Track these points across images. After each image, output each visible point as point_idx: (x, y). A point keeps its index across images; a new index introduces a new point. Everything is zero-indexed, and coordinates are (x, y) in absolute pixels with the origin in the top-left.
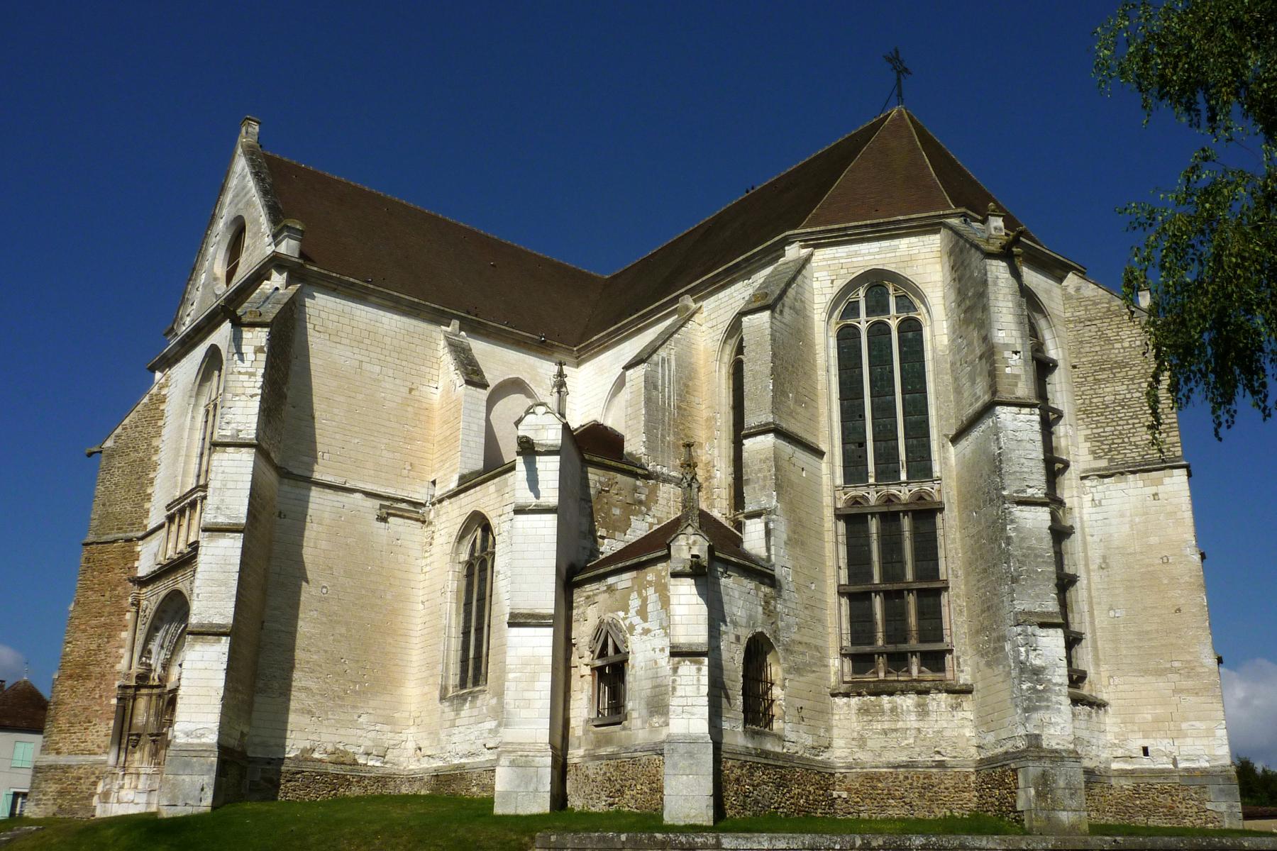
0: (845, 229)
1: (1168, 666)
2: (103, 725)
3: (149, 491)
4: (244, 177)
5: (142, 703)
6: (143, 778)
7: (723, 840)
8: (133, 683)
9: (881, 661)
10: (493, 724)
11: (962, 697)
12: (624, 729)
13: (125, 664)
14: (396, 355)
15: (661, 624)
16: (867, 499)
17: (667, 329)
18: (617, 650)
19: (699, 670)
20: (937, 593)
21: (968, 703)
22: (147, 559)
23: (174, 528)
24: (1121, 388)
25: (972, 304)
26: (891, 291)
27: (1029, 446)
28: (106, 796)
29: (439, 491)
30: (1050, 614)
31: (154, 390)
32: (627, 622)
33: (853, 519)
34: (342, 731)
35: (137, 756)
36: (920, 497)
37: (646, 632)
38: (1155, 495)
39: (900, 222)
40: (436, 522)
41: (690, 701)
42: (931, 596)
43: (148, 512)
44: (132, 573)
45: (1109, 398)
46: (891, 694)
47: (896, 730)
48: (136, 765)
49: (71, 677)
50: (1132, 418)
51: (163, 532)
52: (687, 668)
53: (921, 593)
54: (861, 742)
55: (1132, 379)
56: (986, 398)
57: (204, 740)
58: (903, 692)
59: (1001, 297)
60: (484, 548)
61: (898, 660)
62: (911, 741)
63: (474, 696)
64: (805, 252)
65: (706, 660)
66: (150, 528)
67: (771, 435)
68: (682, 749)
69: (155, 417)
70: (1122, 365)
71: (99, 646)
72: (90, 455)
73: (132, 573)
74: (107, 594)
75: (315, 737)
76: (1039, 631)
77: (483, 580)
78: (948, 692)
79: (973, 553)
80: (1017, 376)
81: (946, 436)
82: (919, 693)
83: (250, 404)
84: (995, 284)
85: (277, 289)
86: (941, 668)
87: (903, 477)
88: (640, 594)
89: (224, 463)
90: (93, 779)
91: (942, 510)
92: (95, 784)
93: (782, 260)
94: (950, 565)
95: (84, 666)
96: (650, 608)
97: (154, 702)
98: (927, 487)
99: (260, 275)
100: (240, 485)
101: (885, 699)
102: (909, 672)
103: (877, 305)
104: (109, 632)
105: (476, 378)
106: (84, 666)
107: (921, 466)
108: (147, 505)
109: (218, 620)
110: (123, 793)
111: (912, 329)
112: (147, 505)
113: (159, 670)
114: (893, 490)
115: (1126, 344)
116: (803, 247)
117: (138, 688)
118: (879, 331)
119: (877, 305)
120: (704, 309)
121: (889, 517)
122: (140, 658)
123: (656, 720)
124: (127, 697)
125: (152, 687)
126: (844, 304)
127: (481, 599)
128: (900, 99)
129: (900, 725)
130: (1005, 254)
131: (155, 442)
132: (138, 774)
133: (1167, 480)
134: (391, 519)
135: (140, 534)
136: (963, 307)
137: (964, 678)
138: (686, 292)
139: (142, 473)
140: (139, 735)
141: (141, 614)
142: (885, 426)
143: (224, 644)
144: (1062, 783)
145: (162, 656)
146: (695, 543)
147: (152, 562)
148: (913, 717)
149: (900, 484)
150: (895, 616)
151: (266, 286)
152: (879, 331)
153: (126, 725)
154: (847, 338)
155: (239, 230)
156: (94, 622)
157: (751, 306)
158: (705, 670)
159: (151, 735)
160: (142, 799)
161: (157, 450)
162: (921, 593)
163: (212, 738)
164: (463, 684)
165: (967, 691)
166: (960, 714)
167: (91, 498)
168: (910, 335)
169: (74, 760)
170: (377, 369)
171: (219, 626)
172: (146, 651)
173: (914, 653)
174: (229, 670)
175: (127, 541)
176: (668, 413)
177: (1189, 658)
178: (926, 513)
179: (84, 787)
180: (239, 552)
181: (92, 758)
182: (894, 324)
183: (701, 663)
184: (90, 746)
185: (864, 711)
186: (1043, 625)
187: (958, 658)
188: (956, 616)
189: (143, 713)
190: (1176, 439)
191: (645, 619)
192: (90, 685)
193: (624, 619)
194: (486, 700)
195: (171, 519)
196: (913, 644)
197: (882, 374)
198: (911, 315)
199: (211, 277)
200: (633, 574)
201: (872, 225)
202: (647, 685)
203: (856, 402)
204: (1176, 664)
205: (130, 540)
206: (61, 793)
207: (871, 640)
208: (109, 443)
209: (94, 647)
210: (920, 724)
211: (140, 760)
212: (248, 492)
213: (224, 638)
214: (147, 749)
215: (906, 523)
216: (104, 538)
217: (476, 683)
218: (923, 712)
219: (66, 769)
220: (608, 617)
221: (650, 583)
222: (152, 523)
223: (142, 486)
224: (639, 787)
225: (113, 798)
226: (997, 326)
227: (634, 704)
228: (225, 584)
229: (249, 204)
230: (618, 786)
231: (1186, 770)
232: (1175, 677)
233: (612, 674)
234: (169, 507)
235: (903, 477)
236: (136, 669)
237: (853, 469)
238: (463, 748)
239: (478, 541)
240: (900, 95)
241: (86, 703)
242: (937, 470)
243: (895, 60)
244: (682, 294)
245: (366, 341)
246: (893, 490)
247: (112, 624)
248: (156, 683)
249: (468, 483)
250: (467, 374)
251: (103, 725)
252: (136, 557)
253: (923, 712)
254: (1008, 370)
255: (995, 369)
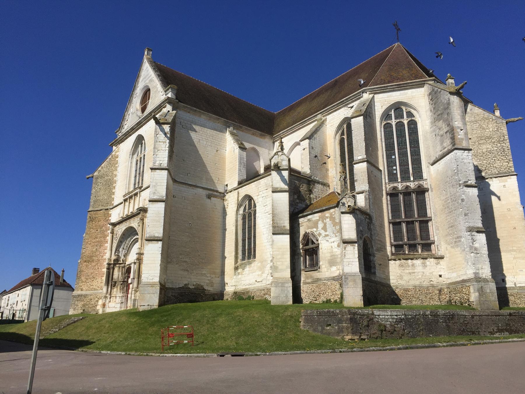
0: (387, 86)
1: (511, 249)
2: (100, 279)
3: (113, 191)
4: (148, 71)
5: (116, 269)
6: (118, 298)
7: (375, 312)
8: (112, 262)
9: (406, 248)
10: (260, 273)
11: (440, 260)
12: (319, 272)
13: (107, 254)
14: (211, 137)
15: (333, 233)
16: (398, 188)
17: (314, 127)
18: (313, 243)
19: (354, 248)
20: (427, 222)
21: (442, 262)
22: (115, 216)
23: (127, 204)
24: (489, 146)
25: (440, 112)
26: (404, 110)
27: (468, 164)
28: (104, 305)
29: (229, 188)
30: (481, 228)
31: (113, 153)
32: (318, 232)
33: (393, 195)
34: (199, 277)
35: (115, 290)
36: (420, 186)
37: (327, 235)
38: (504, 186)
39: (408, 83)
40: (229, 199)
41: (351, 260)
42: (425, 223)
43: (113, 199)
44: (109, 222)
45: (484, 150)
46: (412, 259)
47: (414, 273)
48: (115, 293)
49: (85, 261)
50: (494, 157)
51: (123, 204)
52: (349, 247)
53: (421, 222)
54: (401, 277)
55: (494, 143)
56: (450, 147)
57: (154, 281)
58: (417, 259)
59: (455, 109)
60: (250, 208)
61: (413, 247)
62: (420, 276)
63: (250, 263)
64: (371, 96)
65: (356, 245)
66: (115, 205)
67: (366, 163)
68: (350, 278)
69: (114, 164)
70: (489, 138)
71: (96, 249)
72: (88, 178)
73: (109, 222)
74: (99, 230)
75: (189, 280)
76: (476, 234)
77: (250, 220)
78: (434, 258)
79: (443, 206)
80: (462, 139)
81: (429, 163)
82: (423, 259)
83: (164, 153)
84: (453, 104)
85: (169, 111)
86: (430, 250)
87: (412, 179)
88: (323, 221)
89: (156, 176)
90: (96, 299)
91: (428, 191)
92: (97, 301)
93: (361, 99)
94: (432, 211)
95: (91, 257)
96: (328, 226)
97: (121, 270)
98: (421, 182)
99: (160, 107)
100: (162, 184)
101: (410, 261)
102: (417, 251)
103: (399, 115)
104: (101, 244)
105: (242, 146)
106: (91, 257)
107: (418, 174)
108: (113, 196)
109: (157, 235)
110: (110, 304)
111: (413, 125)
112: (113, 196)
113: (122, 257)
114: (408, 184)
115: (491, 130)
116: (370, 94)
117: (115, 264)
118: (400, 125)
119: (399, 115)
120: (327, 119)
121: (407, 193)
122: (115, 253)
123: (334, 268)
124: (110, 268)
125: (120, 264)
126: (386, 115)
127: (250, 227)
128: (398, 40)
129: (415, 271)
130: (457, 93)
131: (115, 173)
132: (116, 297)
133: (509, 180)
134: (212, 198)
135: (111, 207)
136: (437, 114)
137: (440, 253)
138: (320, 113)
139: (110, 185)
140: (115, 282)
141: (115, 236)
142: (404, 160)
143: (160, 244)
144: (488, 291)
145: (123, 252)
146: (349, 201)
147: (118, 217)
148: (421, 268)
149: (411, 181)
150: (411, 231)
151: (165, 110)
152: (400, 125)
153: (110, 279)
154: (387, 128)
155: (147, 93)
156: (94, 241)
157: (355, 115)
158: (356, 248)
159: (120, 282)
160: (119, 305)
161: (116, 176)
162: (421, 222)
163: (157, 280)
164: (243, 259)
165: (442, 258)
166: (439, 266)
167: (90, 194)
168: (412, 126)
169: (88, 292)
170: (205, 143)
171: (157, 237)
172: (117, 250)
173: (419, 244)
174: (162, 254)
175: (106, 210)
176: (318, 159)
177: (520, 246)
178: (421, 192)
179: (93, 302)
180: (163, 209)
181: (96, 291)
182: (394, 124)
183: (355, 246)
184: (95, 287)
185: (401, 266)
186: (478, 232)
187: (437, 245)
188: (437, 231)
189: (117, 274)
190: (512, 165)
191: (326, 231)
192: (93, 264)
193: (316, 231)
194: (256, 264)
195: (125, 200)
196: (419, 240)
197: (402, 141)
198: (413, 118)
199: (133, 113)
200: (320, 214)
201: (397, 85)
202: (328, 255)
203: (392, 152)
204: (514, 248)
205: (107, 209)
206: (84, 305)
207: (402, 239)
208: (96, 174)
209: (94, 250)
210: (424, 270)
211: (117, 292)
212: (166, 187)
213: (160, 242)
214: (119, 287)
215: (414, 196)
216: (96, 209)
217: (249, 258)
218: (424, 266)
219: (85, 296)
220: (308, 231)
221: (327, 217)
222: (116, 203)
223: (110, 189)
224: (327, 293)
225: (107, 306)
226: (454, 120)
227: (323, 263)
228: (159, 222)
229: (151, 81)
230: (318, 294)
231: (520, 287)
232: (515, 253)
233: (313, 252)
234: (124, 196)
235: (412, 179)
236: (114, 257)
237: (392, 177)
238: (248, 282)
239: (247, 206)
240: (398, 39)
241: (92, 271)
242: (425, 176)
243: (395, 25)
244: (318, 114)
245: (201, 132)
246: (408, 184)
247: (101, 241)
248: (121, 262)
249: (241, 183)
250: (239, 144)
251: (100, 279)
252: (110, 216)
253: (424, 266)
254: (459, 136)
255: (454, 136)
